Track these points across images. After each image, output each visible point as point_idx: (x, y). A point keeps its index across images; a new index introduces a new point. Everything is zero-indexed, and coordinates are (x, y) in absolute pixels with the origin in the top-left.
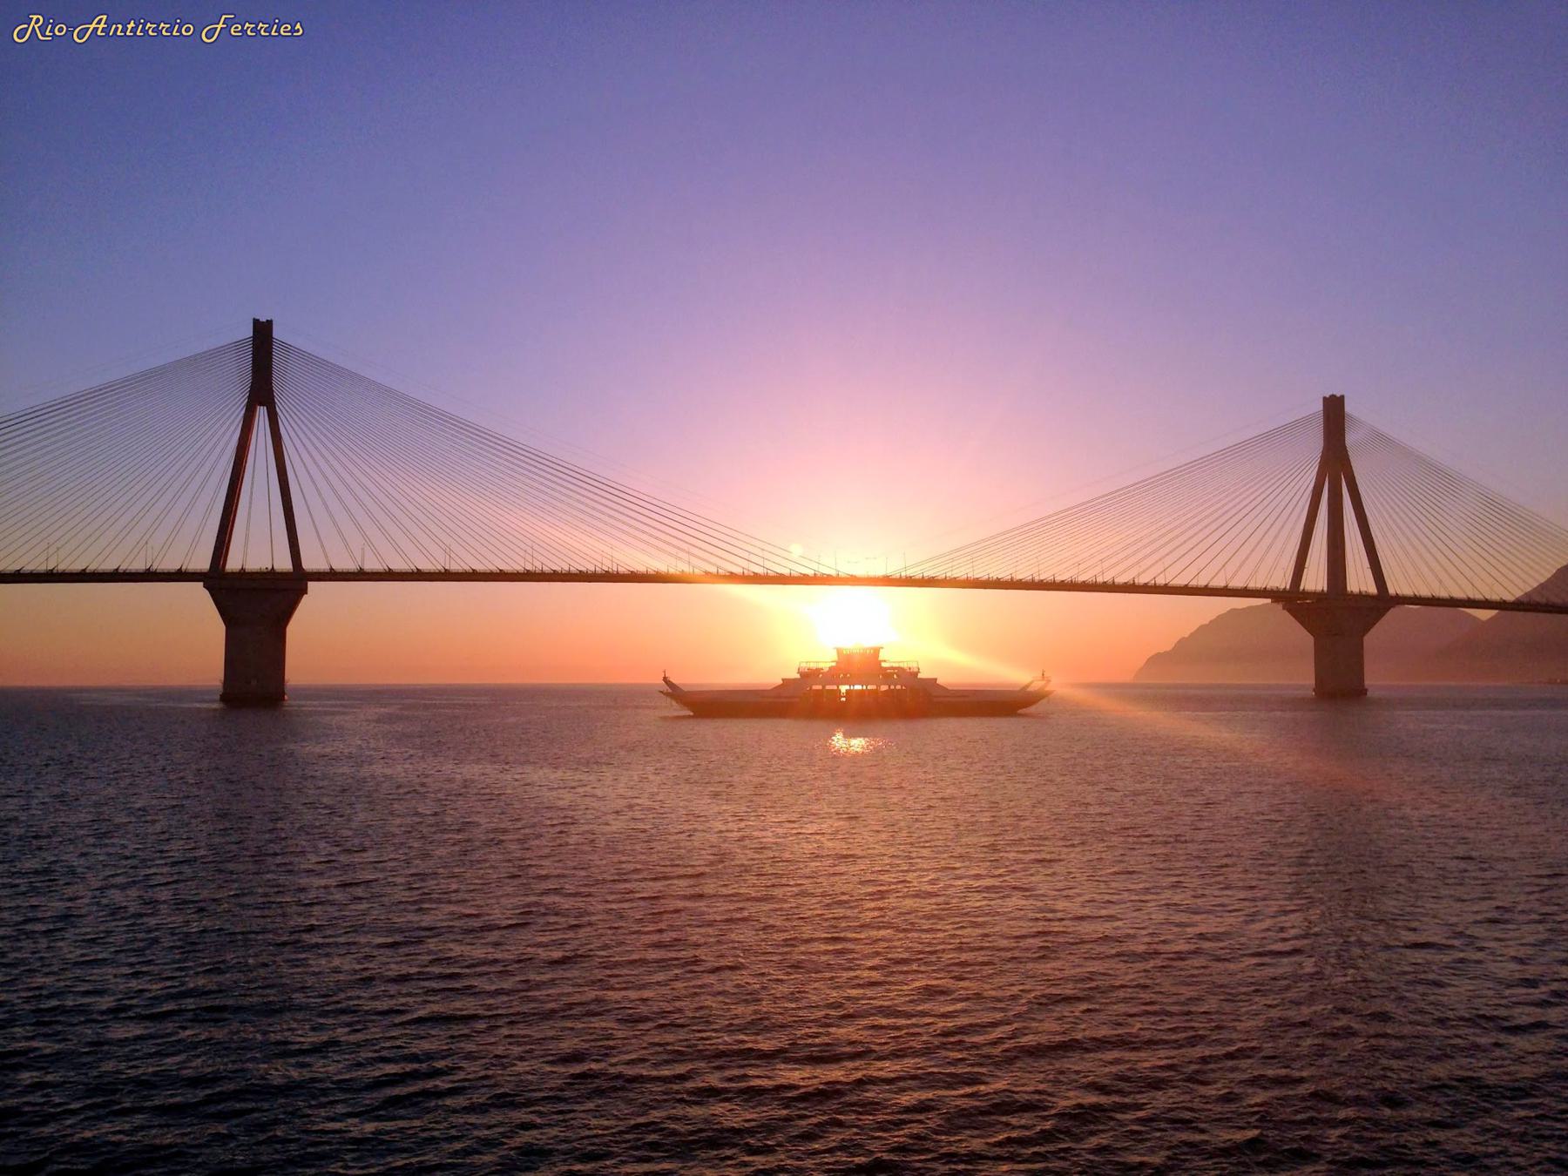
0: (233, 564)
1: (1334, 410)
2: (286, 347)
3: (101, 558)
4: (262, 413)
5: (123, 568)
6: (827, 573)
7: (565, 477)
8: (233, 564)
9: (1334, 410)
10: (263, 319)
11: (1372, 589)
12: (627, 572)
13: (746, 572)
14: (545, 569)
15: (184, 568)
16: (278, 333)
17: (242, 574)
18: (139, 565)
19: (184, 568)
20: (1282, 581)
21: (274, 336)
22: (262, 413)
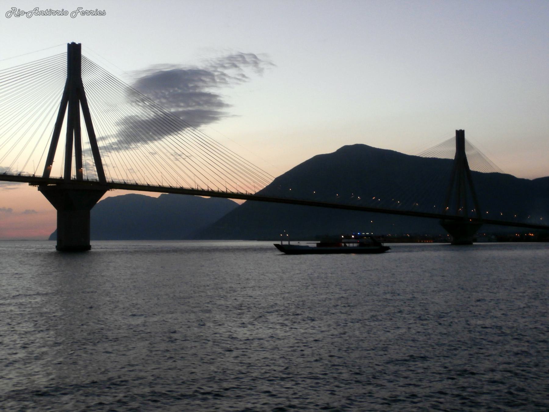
1: (460, 135)
2: (91, 64)
6: (232, 191)
9: (460, 135)
10: (77, 43)
13: (209, 189)
16: (84, 52)
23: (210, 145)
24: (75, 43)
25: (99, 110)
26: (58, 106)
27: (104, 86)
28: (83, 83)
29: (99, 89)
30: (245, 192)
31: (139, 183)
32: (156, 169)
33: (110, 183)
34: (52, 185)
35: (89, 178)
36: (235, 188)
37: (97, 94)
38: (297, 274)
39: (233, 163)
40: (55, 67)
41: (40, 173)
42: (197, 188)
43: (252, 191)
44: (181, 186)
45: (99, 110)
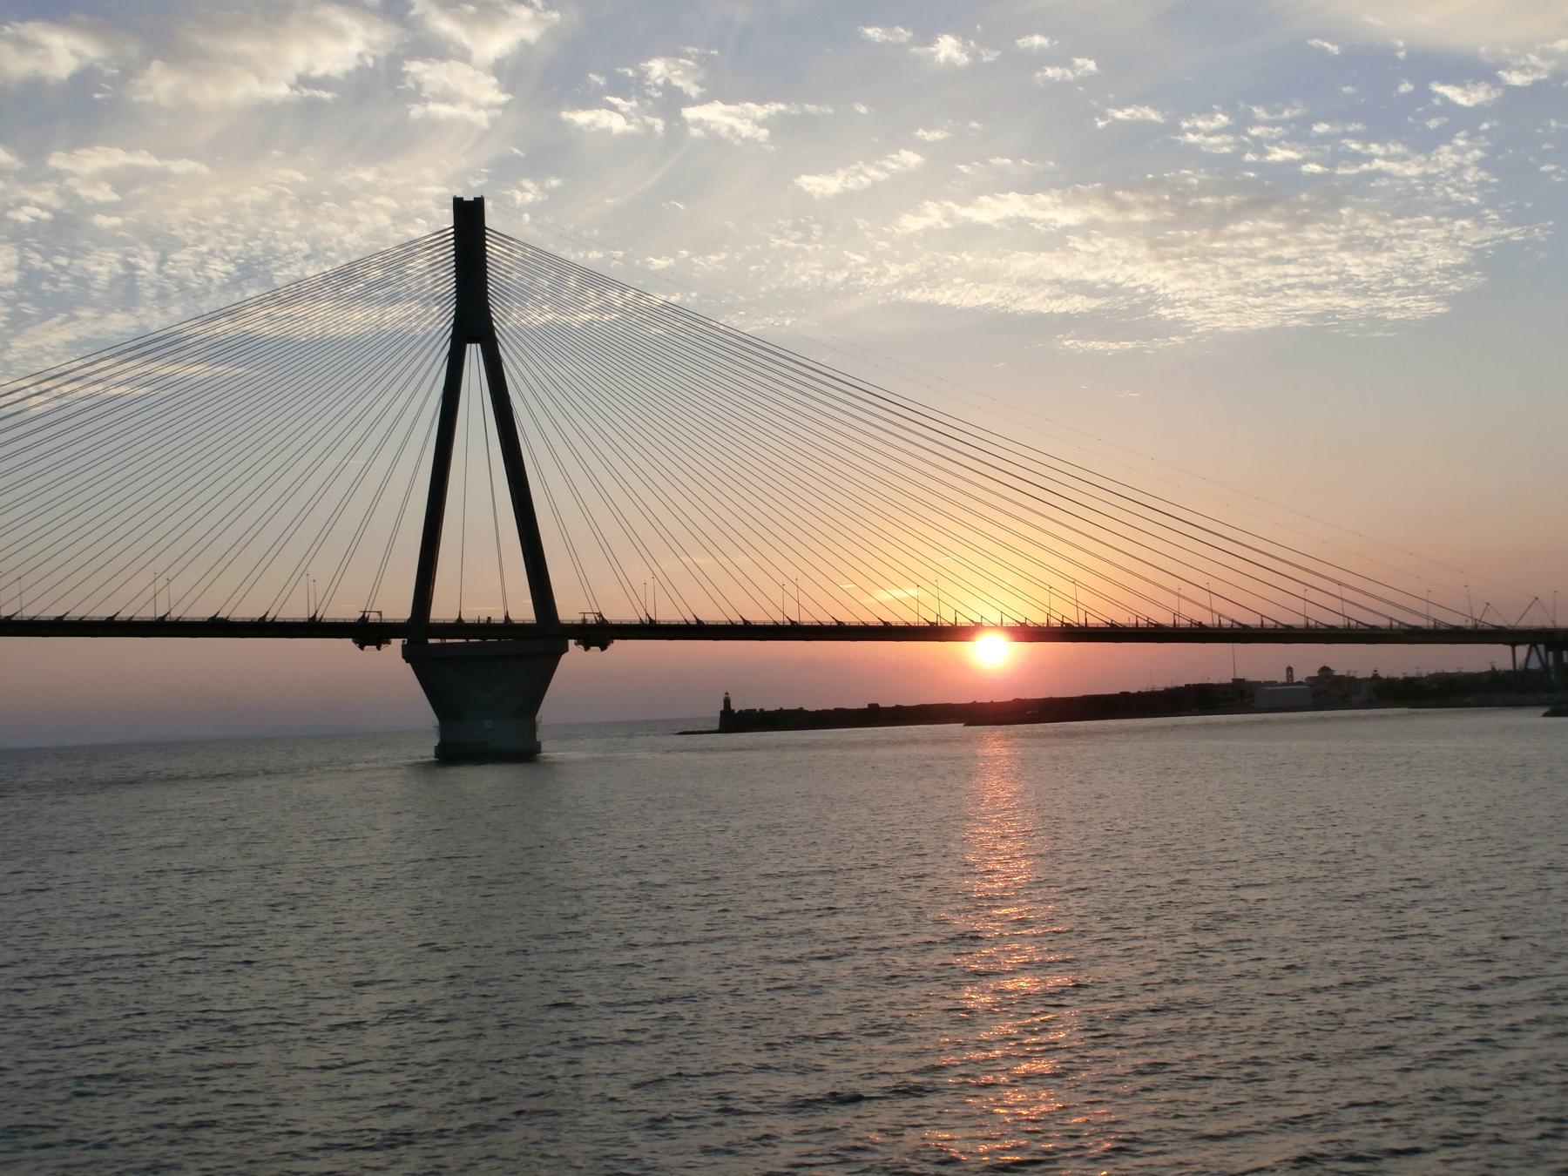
0: (442, 610)
1: (469, 215)
3: (235, 600)
4: (474, 354)
5: (175, 615)
7: (675, 441)
8: (442, 610)
9: (469, 215)
10: (469, 198)
11: (523, 610)
12: (1102, 625)
13: (1140, 621)
14: (1267, 623)
15: (318, 616)
16: (492, 220)
17: (459, 627)
18: (201, 611)
19: (318, 616)
20: (569, 609)
21: (487, 224)
22: (474, 354)
23: (880, 428)
24: (462, 199)
25: (369, 356)
26: (435, 414)
27: (808, 412)
28: (495, 324)
29: (799, 418)
30: (1432, 623)
31: (894, 620)
32: (320, 541)
33: (591, 626)
34: (448, 641)
35: (462, 617)
36: (1207, 608)
37: (520, 348)
38: (1336, 937)
39: (892, 471)
40: (224, 389)
41: (399, 608)
42: (1217, 622)
43: (606, 618)
44: (1023, 621)
45: (369, 356)
